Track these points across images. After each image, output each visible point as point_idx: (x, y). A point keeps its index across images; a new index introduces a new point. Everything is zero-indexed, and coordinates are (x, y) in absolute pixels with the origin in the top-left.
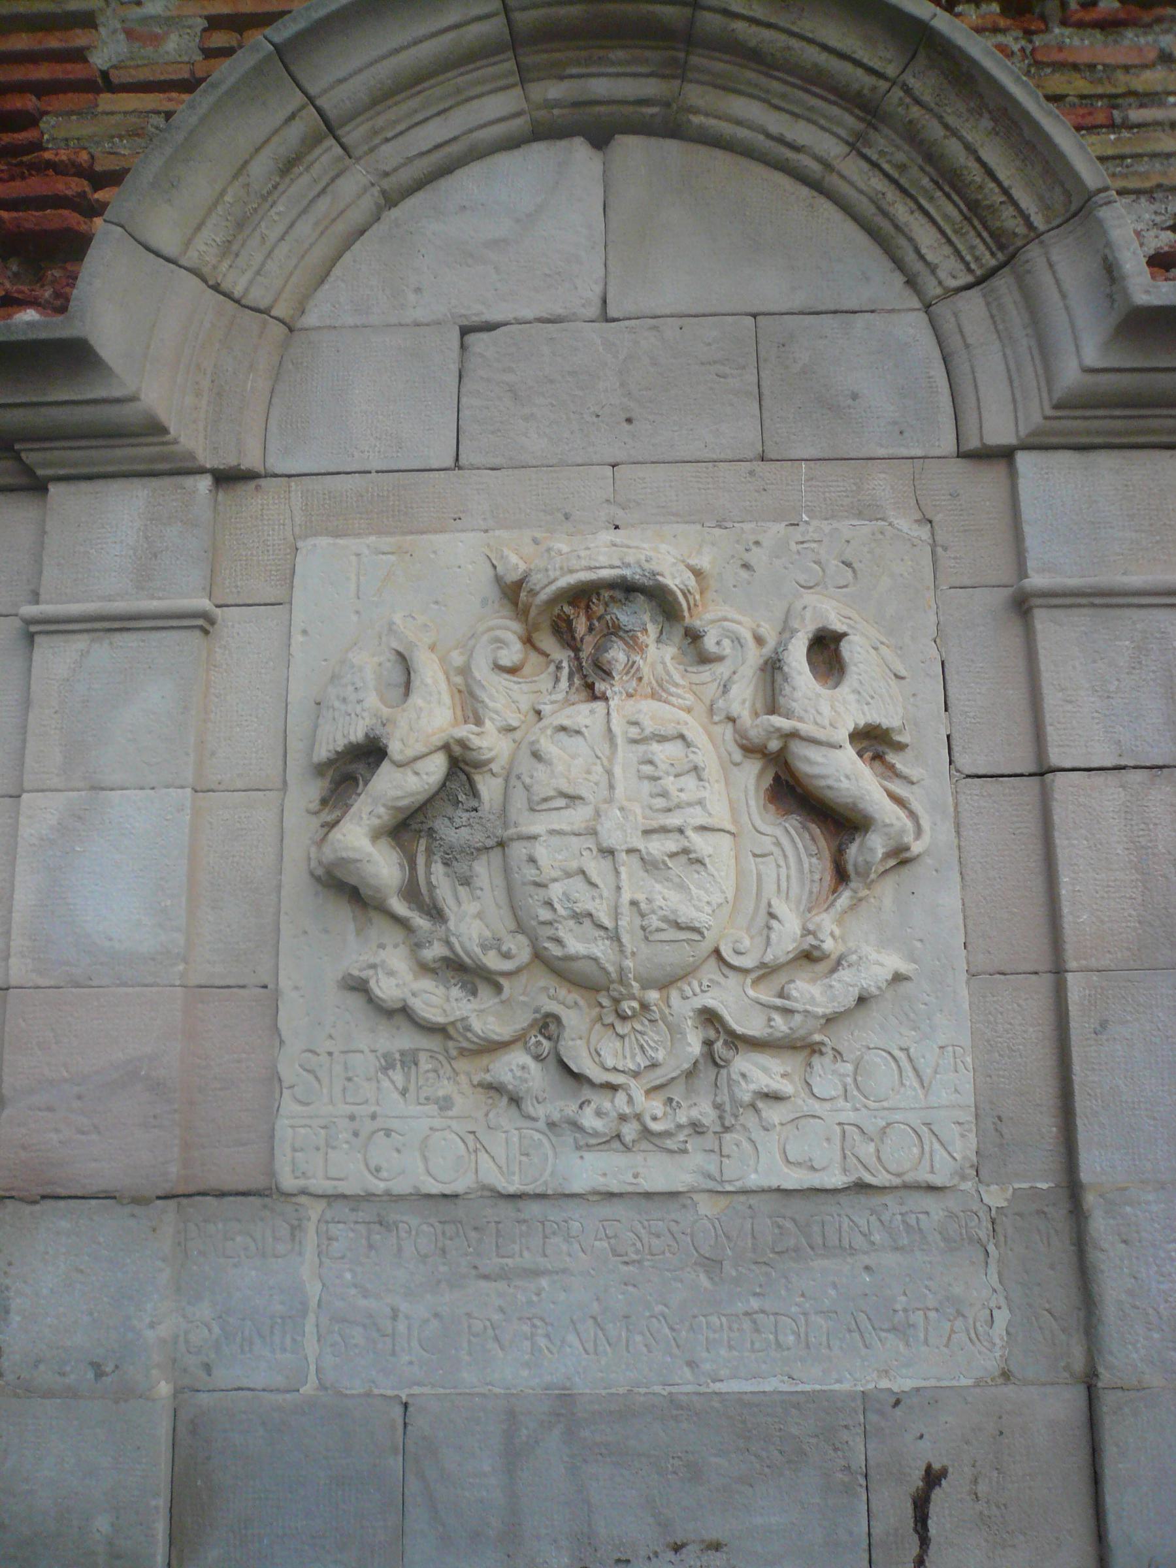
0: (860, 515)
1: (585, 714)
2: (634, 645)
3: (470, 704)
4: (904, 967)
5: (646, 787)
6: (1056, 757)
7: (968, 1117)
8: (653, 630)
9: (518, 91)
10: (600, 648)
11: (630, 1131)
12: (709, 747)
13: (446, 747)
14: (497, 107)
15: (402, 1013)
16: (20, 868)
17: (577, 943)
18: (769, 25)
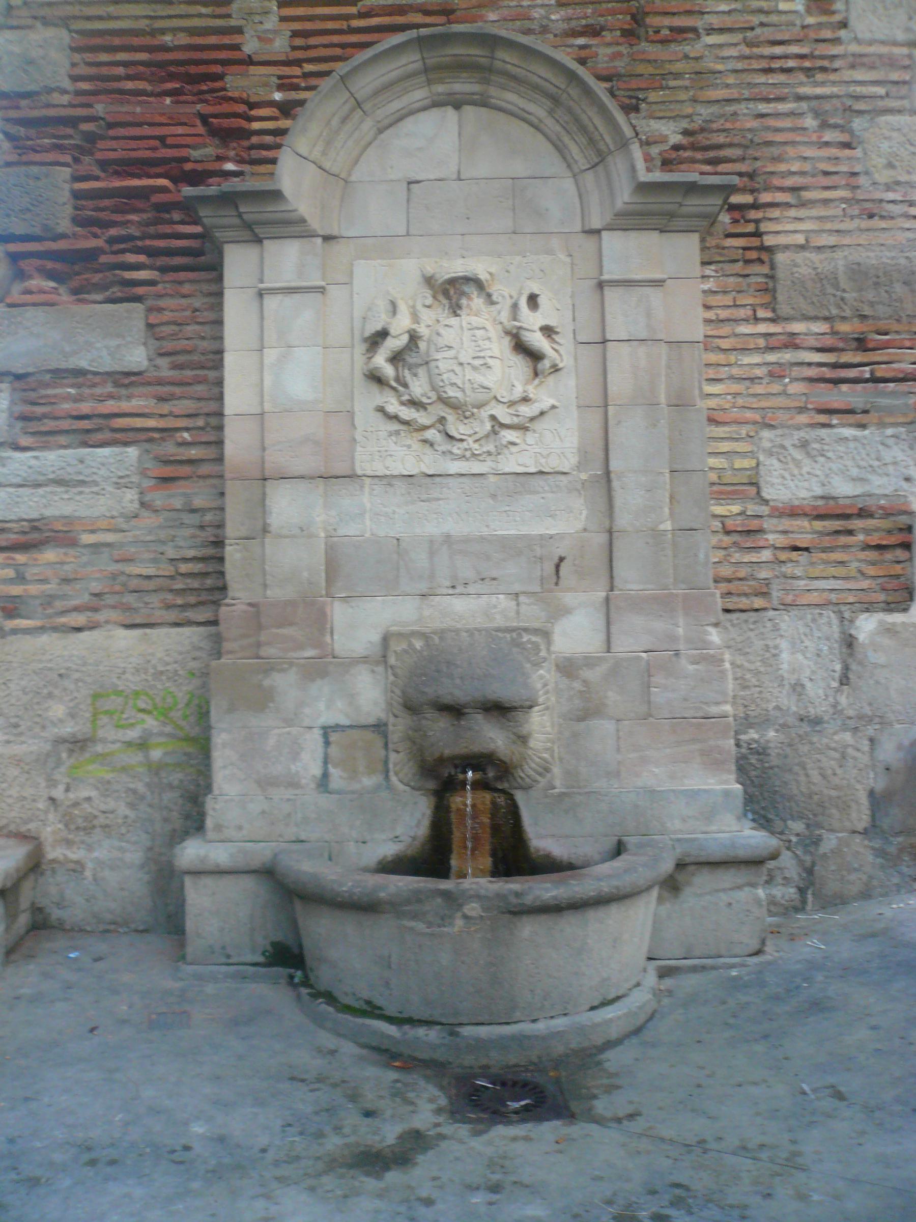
0: (547, 253)
1: (453, 321)
2: (470, 298)
3: (415, 318)
4: (556, 404)
5: (473, 344)
6: (609, 336)
7: (575, 451)
8: (476, 293)
9: (426, 88)
10: (459, 299)
11: (468, 454)
12: (494, 332)
13: (408, 332)
14: (419, 95)
15: (395, 418)
16: (265, 373)
17: (451, 393)
18: (519, 67)
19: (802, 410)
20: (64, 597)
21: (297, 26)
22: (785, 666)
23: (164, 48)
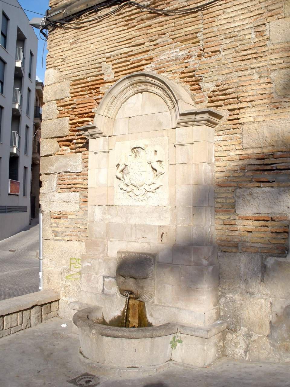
11: (140, 200)
14: (131, 91)
19: (251, 182)
20: (65, 232)
21: (116, 70)
22: (242, 273)
23: (88, 82)
